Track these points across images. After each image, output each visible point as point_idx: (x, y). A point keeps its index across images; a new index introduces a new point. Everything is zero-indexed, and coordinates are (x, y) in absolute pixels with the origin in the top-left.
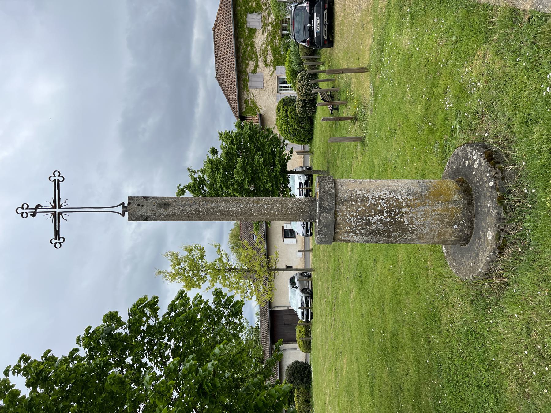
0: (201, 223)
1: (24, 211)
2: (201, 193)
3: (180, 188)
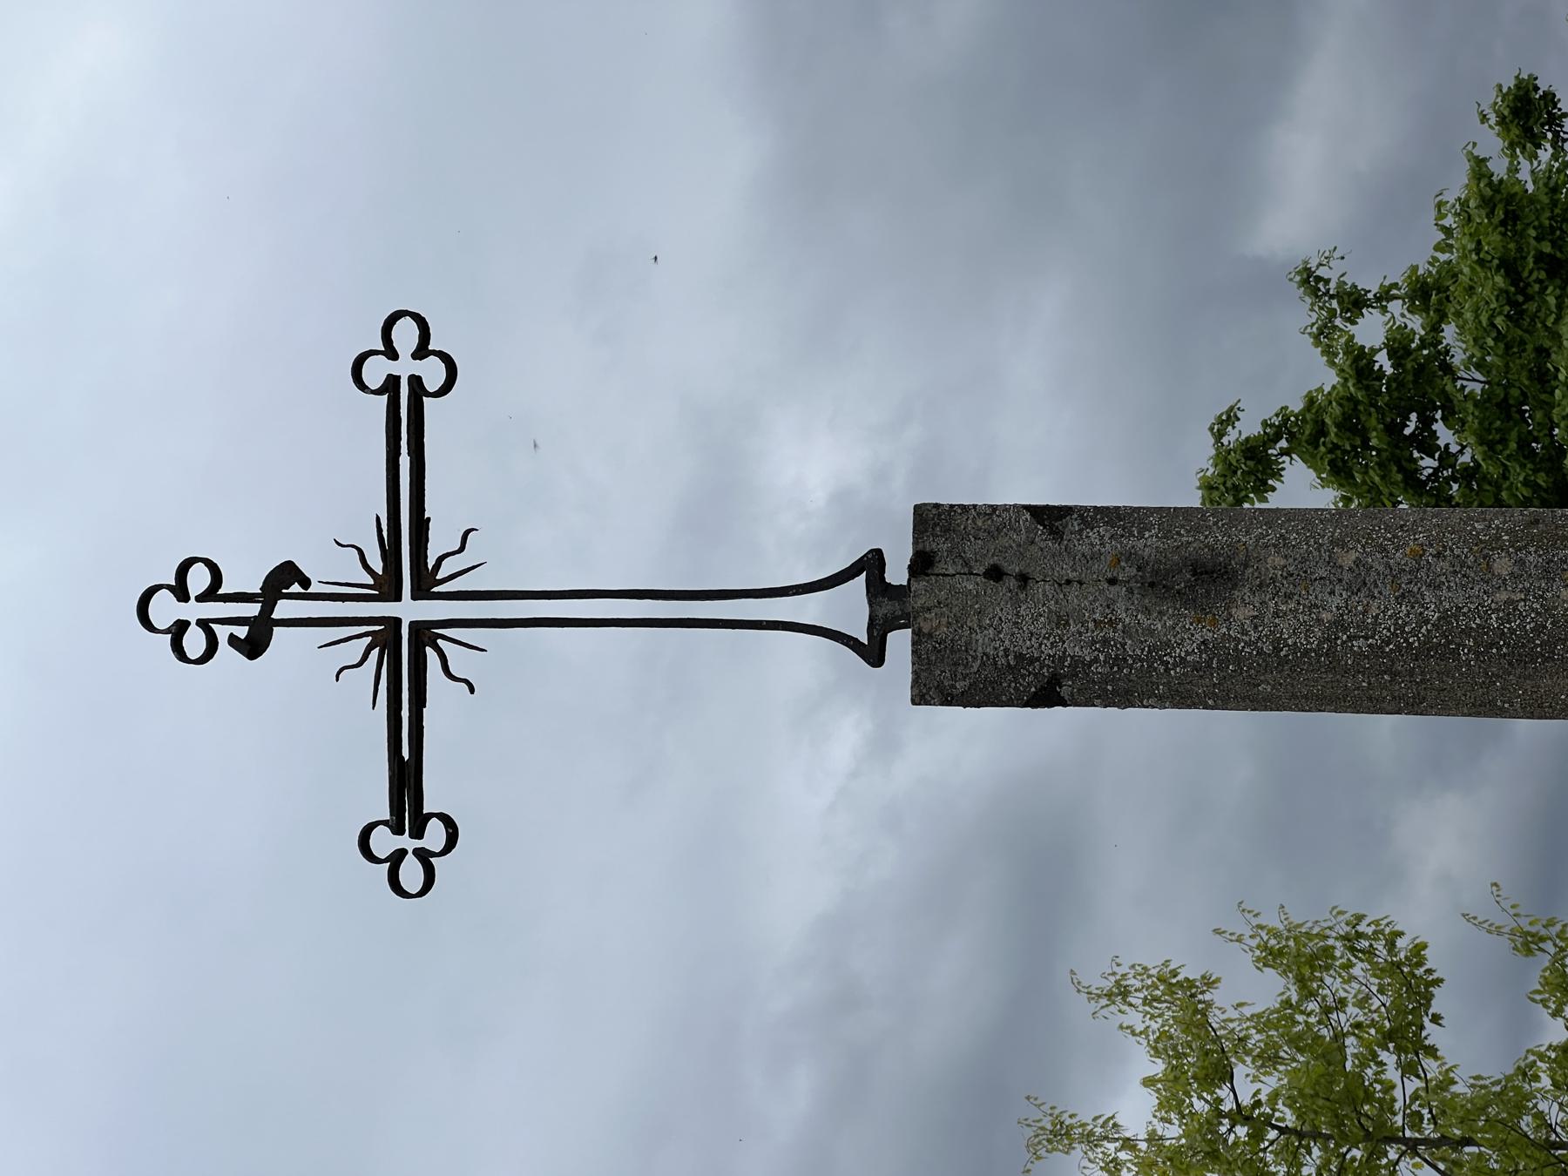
0: (1384, 734)
1: (193, 611)
2: (1413, 482)
3: (1231, 437)
